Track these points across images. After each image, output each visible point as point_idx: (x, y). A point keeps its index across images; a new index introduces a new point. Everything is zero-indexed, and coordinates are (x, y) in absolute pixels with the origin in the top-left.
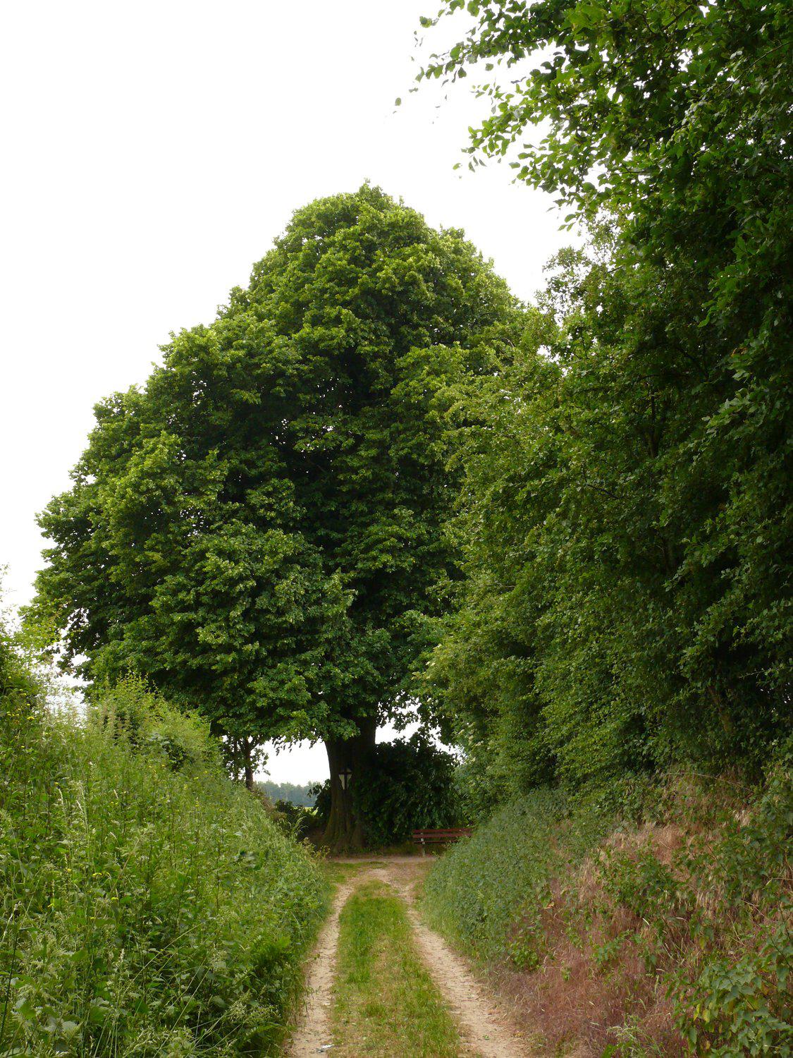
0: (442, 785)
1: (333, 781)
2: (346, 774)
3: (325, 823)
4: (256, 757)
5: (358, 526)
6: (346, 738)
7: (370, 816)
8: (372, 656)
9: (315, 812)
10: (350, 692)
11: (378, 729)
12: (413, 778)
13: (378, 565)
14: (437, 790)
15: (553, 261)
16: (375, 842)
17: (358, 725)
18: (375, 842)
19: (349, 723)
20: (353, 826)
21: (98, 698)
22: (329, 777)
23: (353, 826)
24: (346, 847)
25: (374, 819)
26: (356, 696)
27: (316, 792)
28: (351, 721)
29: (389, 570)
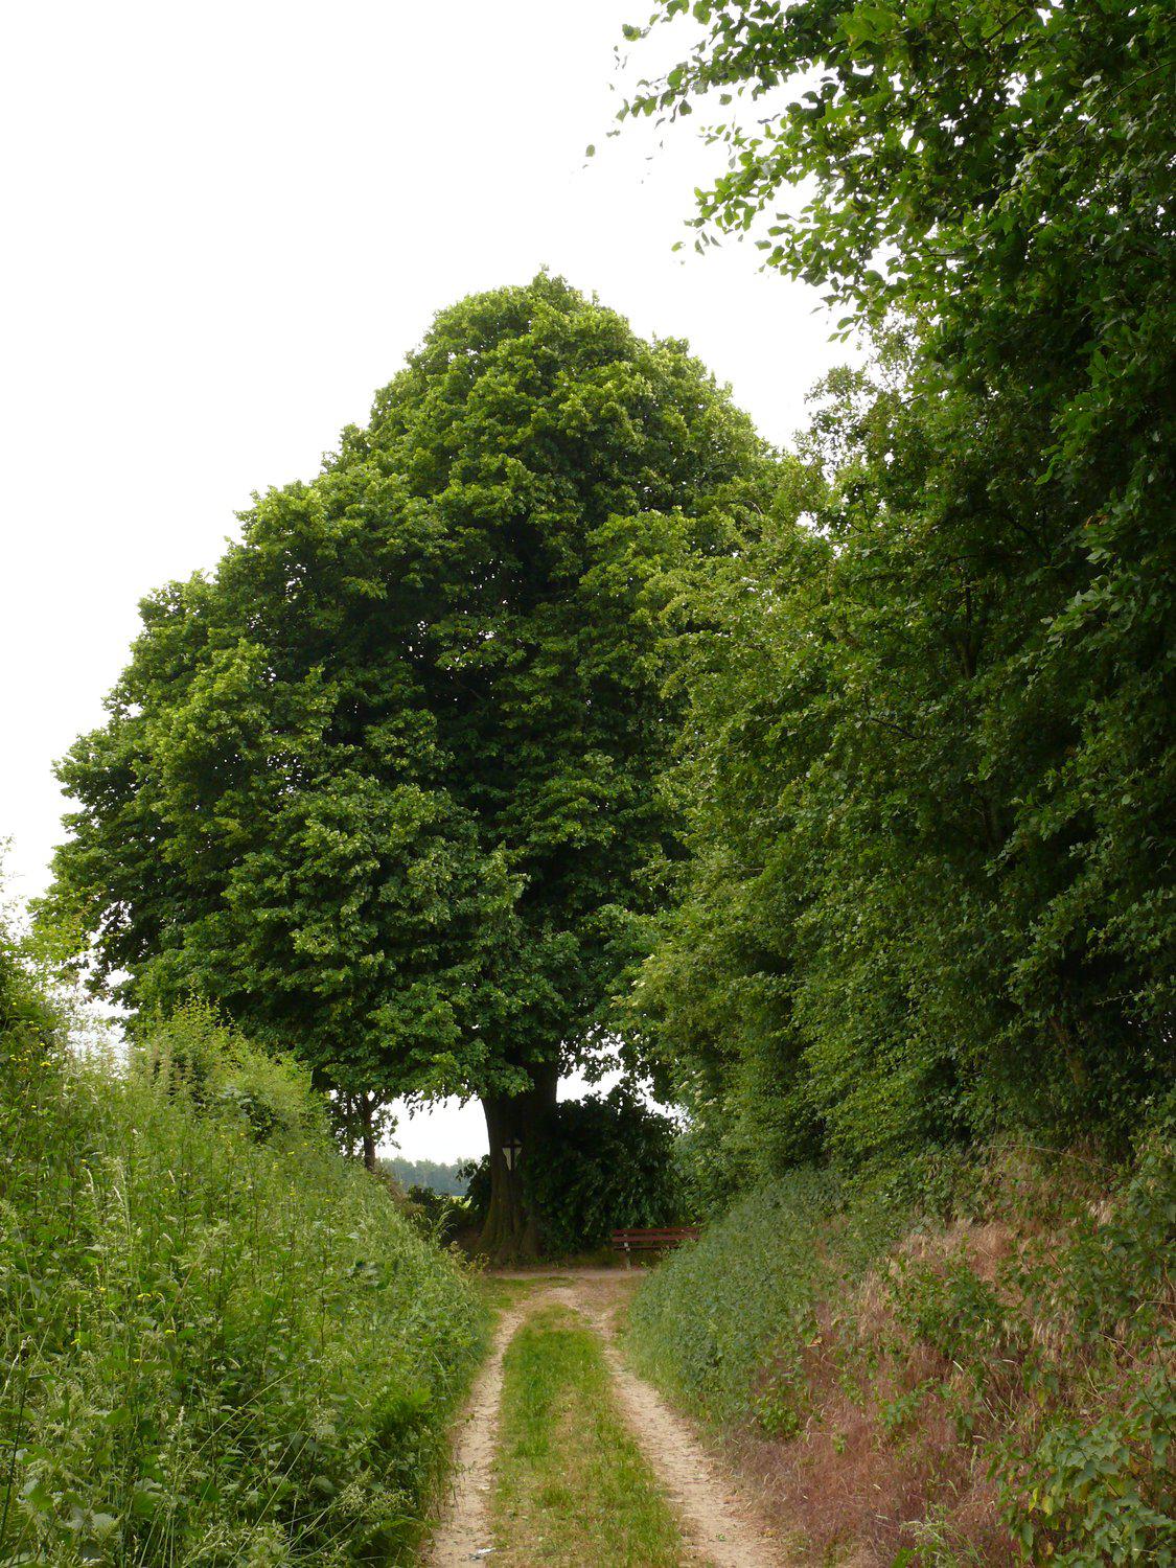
0: (656, 1164)
1: (494, 1158)
2: (513, 1147)
3: (482, 1220)
4: (380, 1123)
5: (531, 779)
6: (513, 1093)
7: (549, 1209)
9: (467, 1204)
10: (519, 1025)
11: (561, 1081)
12: (613, 1154)
13: (561, 837)
14: (649, 1171)
15: (819, 386)
16: (556, 1248)
17: (530, 1075)
18: (556, 1248)
19: (517, 1072)
20: (524, 1225)
22: (487, 1151)
23: (524, 1225)
24: (513, 1255)
25: (554, 1214)
26: (527, 1031)
27: (469, 1174)
28: (520, 1069)
29: (577, 845)
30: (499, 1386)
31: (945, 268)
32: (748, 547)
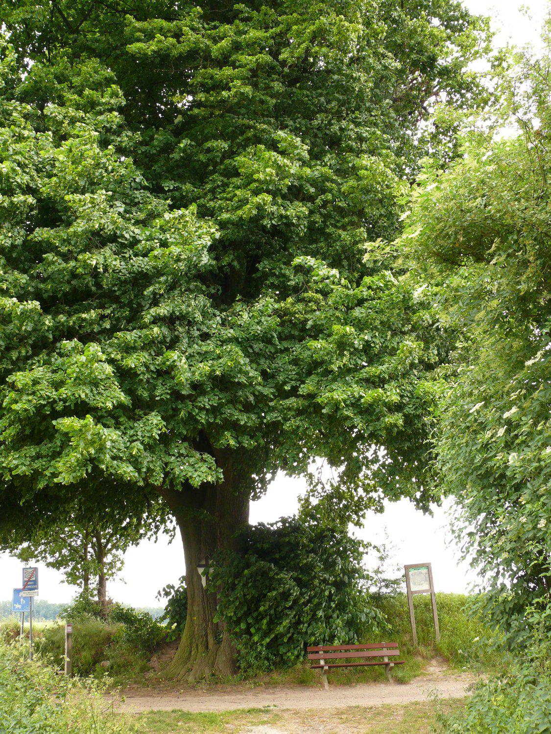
0: (346, 579)
1: (191, 577)
2: (206, 566)
3: (179, 638)
4: (112, 565)
5: (222, 174)
6: (196, 482)
7: (243, 626)
8: (244, 344)
9: (164, 624)
10: (205, 401)
11: (252, 505)
12: (310, 567)
13: (247, 212)
14: (340, 585)
15: (269, 483)
16: (250, 666)
17: (219, 464)
18: (250, 666)
19: (203, 460)
20: (219, 642)
21: (389, 709)
22: (182, 571)
23: (219, 642)
24: (207, 673)
25: (248, 631)
26: (214, 411)
27: (167, 594)
28: (206, 456)
29: (266, 222)
30: (224, 659)
31: (406, 175)
32: (373, 137)
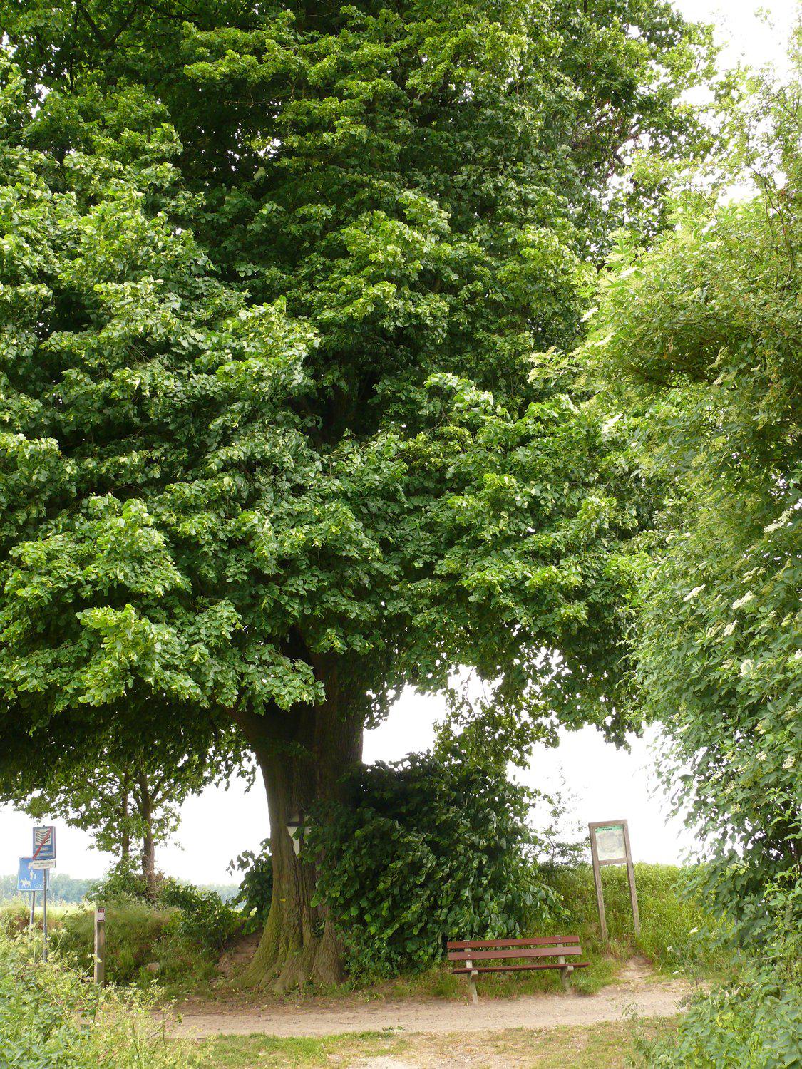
0: (504, 843)
1: (277, 841)
2: (300, 824)
3: (260, 930)
4: (162, 823)
5: (323, 254)
6: (286, 702)
7: (354, 912)
8: (355, 501)
9: (238, 909)
10: (299, 585)
11: (367, 735)
12: (451, 826)
13: (360, 308)
14: (494, 853)
15: (392, 704)
16: (363, 970)
17: (318, 675)
18: (363, 970)
19: (296, 671)
20: (318, 935)
22: (265, 831)
23: (318, 935)
24: (302, 980)
25: (360, 920)
26: (312, 598)
27: (243, 865)
28: (300, 664)
29: (387, 324)
